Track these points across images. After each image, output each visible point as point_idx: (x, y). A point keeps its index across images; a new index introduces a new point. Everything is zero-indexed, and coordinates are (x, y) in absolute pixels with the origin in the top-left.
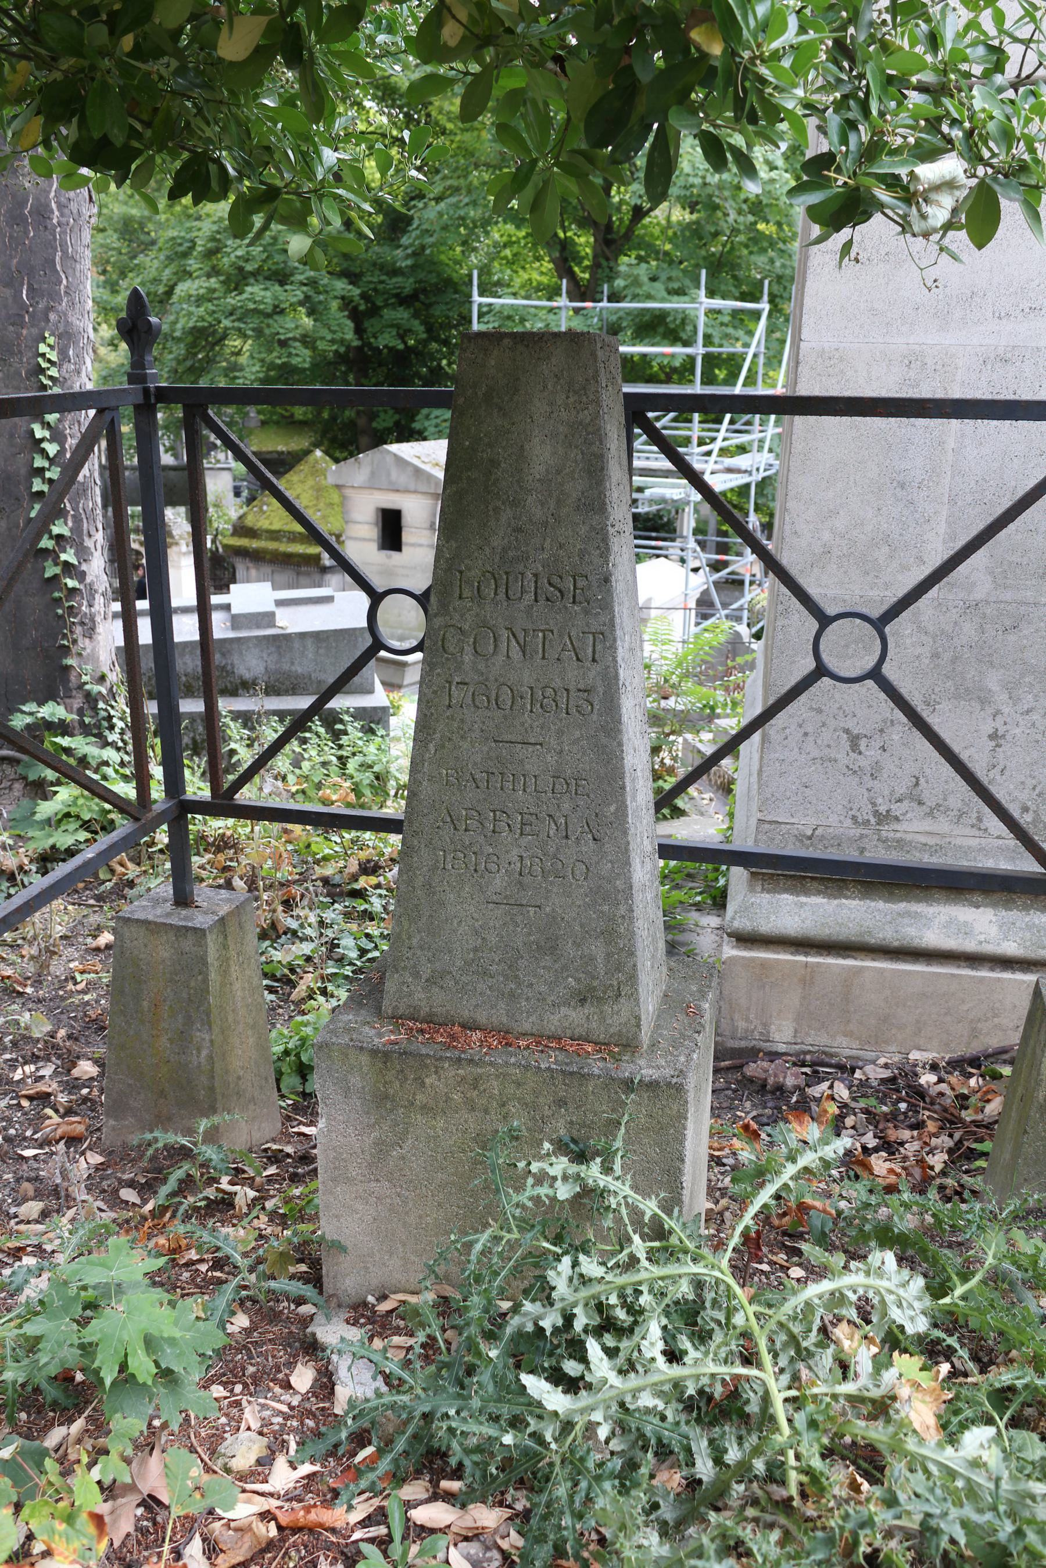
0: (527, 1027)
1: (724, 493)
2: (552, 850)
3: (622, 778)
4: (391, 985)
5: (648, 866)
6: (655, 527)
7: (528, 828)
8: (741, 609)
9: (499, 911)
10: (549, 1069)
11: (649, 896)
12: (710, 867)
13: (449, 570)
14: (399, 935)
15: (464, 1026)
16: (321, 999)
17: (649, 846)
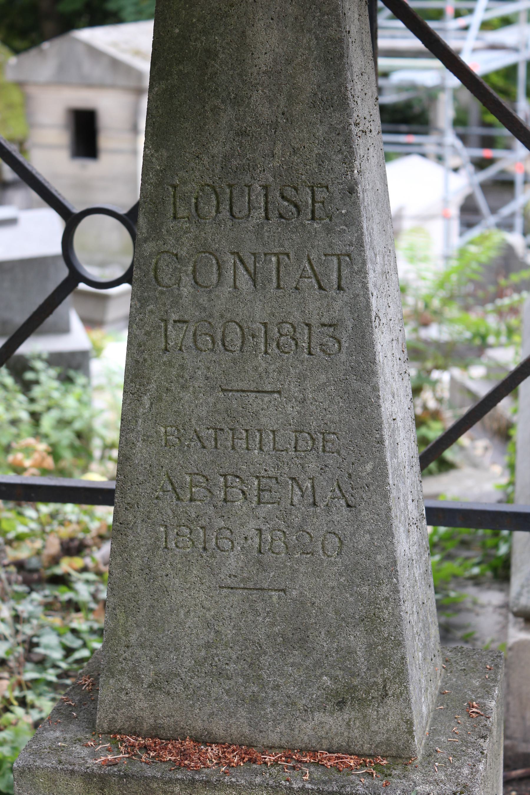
0: (274, 738)
1: (486, 77)
2: (297, 521)
3: (379, 430)
4: (105, 694)
5: (415, 535)
6: (407, 118)
7: (266, 496)
8: (513, 215)
9: (236, 597)
10: (303, 789)
11: (417, 572)
12: (489, 532)
13: (159, 184)
14: (114, 631)
15: (197, 740)
16: (19, 711)
17: (414, 511)
